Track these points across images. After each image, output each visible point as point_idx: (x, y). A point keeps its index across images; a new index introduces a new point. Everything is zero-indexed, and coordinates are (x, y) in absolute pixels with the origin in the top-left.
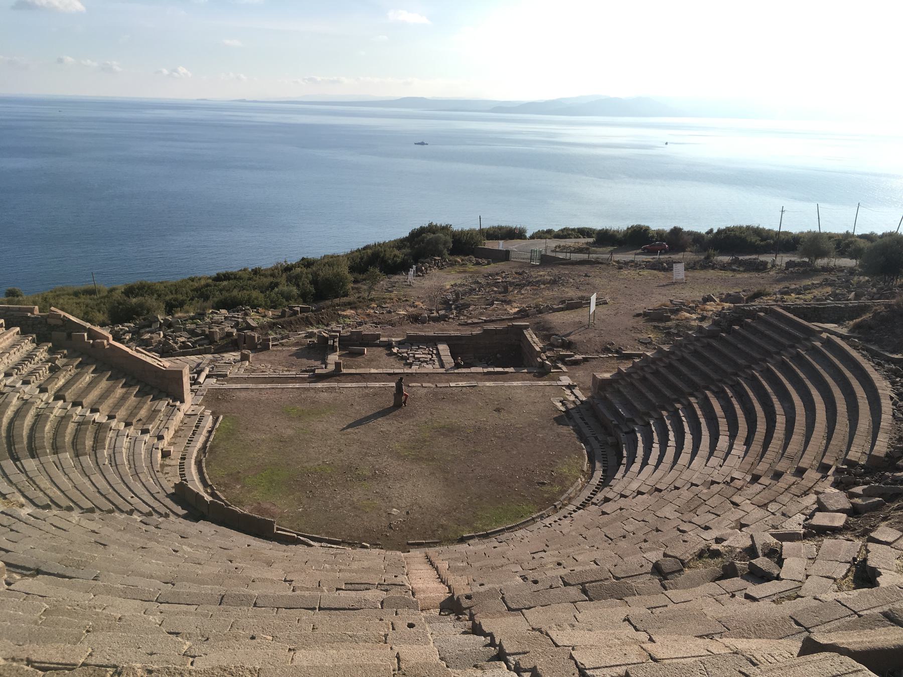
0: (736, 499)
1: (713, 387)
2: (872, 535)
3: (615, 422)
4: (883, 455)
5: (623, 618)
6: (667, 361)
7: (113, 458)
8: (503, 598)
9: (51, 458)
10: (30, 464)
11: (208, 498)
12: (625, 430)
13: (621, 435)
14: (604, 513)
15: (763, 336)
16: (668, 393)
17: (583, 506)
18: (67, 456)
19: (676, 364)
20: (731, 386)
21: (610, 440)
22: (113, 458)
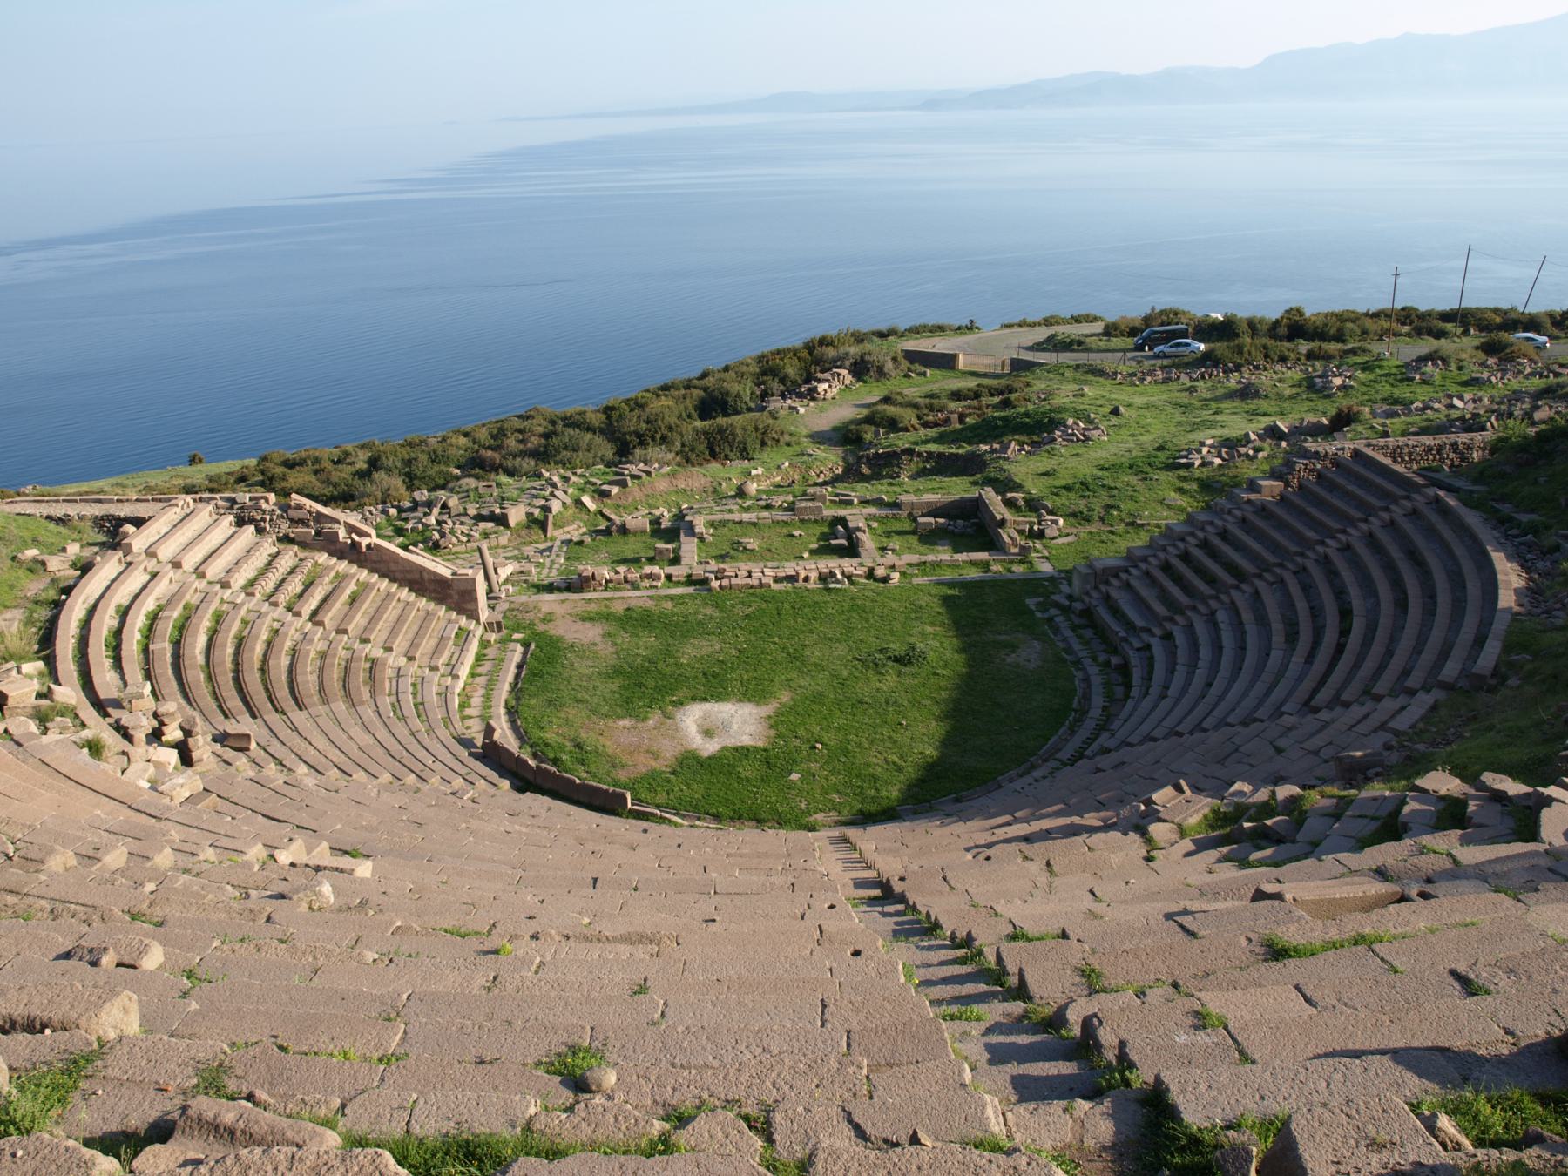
0: (1281, 743)
1: (1289, 565)
2: (1418, 782)
3: (1122, 634)
4: (1488, 673)
5: (1249, 1066)
6: (1200, 534)
7: (397, 706)
8: (944, 878)
9: (323, 709)
10: (298, 717)
11: (532, 763)
12: (1137, 644)
13: (1131, 653)
14: (1099, 770)
15: (1346, 494)
16: (1310, 534)
17: (1073, 761)
18: (340, 706)
19: (1216, 541)
20: (1295, 573)
21: (1115, 660)
22: (397, 706)
